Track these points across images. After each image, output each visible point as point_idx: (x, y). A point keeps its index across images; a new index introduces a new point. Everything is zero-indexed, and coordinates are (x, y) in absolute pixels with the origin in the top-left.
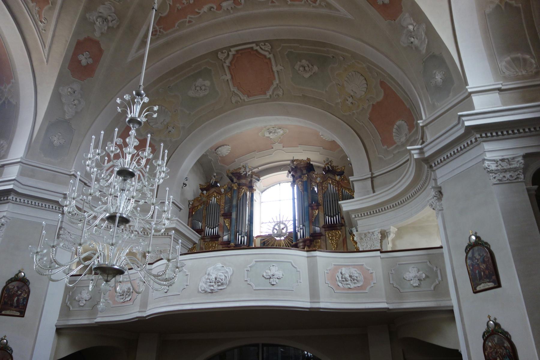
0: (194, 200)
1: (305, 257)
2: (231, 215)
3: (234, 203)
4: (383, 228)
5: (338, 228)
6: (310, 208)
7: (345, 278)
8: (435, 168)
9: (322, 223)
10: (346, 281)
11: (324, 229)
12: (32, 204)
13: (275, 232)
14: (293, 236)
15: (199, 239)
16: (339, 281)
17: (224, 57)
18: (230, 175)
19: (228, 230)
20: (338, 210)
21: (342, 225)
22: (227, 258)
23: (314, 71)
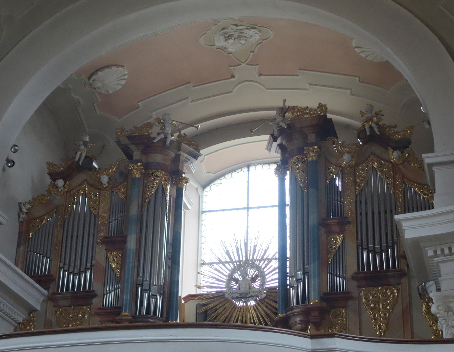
0: (32, 202)
2: (124, 242)
3: (134, 211)
5: (393, 281)
6: (323, 230)
9: (351, 268)
11: (354, 283)
13: (235, 286)
14: (279, 298)
15: (42, 299)
19: (117, 280)
21: (402, 274)
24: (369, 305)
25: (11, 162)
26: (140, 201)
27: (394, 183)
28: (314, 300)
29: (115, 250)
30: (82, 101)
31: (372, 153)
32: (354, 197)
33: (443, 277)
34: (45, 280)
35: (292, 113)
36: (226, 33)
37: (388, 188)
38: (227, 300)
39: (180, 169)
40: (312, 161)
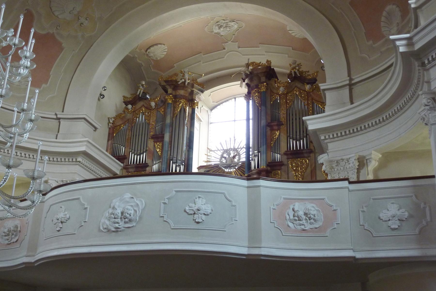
0: (115, 118)
1: (244, 187)
2: (163, 137)
3: (168, 121)
4: (361, 154)
5: (306, 155)
6: (268, 129)
7: (298, 217)
8: (428, 67)
9: (284, 148)
10: (300, 220)
11: (285, 157)
12: (29, 158)
13: (224, 161)
14: (246, 165)
15: (120, 168)
16: (290, 220)
18: (163, 83)
19: (160, 157)
20: (304, 132)
21: (311, 151)
22: (138, 186)
24: (293, 168)
25: (102, 96)
26: (172, 116)
27: (308, 103)
28: (263, 166)
29: (159, 142)
30: (143, 64)
31: (296, 87)
32: (286, 111)
33: (329, 151)
34: (122, 159)
35: (253, 66)
37: (304, 105)
38: (220, 168)
39: (194, 98)
40: (263, 91)
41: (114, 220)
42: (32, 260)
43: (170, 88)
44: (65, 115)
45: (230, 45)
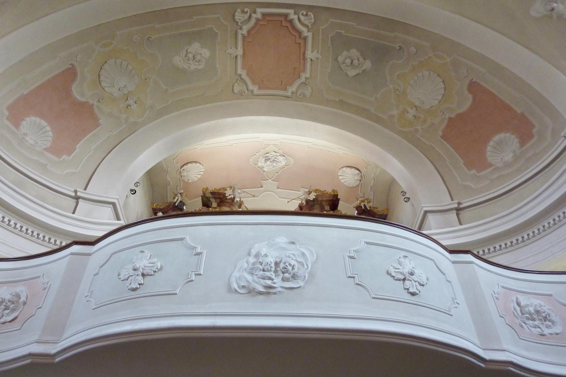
17: (243, 19)
23: (364, 68)
30: (171, 183)
36: (267, 157)
41: (262, 272)
42: (52, 349)
43: (216, 202)
44: (89, 194)
45: (270, 184)
